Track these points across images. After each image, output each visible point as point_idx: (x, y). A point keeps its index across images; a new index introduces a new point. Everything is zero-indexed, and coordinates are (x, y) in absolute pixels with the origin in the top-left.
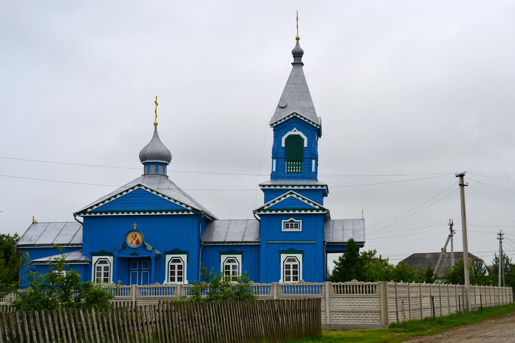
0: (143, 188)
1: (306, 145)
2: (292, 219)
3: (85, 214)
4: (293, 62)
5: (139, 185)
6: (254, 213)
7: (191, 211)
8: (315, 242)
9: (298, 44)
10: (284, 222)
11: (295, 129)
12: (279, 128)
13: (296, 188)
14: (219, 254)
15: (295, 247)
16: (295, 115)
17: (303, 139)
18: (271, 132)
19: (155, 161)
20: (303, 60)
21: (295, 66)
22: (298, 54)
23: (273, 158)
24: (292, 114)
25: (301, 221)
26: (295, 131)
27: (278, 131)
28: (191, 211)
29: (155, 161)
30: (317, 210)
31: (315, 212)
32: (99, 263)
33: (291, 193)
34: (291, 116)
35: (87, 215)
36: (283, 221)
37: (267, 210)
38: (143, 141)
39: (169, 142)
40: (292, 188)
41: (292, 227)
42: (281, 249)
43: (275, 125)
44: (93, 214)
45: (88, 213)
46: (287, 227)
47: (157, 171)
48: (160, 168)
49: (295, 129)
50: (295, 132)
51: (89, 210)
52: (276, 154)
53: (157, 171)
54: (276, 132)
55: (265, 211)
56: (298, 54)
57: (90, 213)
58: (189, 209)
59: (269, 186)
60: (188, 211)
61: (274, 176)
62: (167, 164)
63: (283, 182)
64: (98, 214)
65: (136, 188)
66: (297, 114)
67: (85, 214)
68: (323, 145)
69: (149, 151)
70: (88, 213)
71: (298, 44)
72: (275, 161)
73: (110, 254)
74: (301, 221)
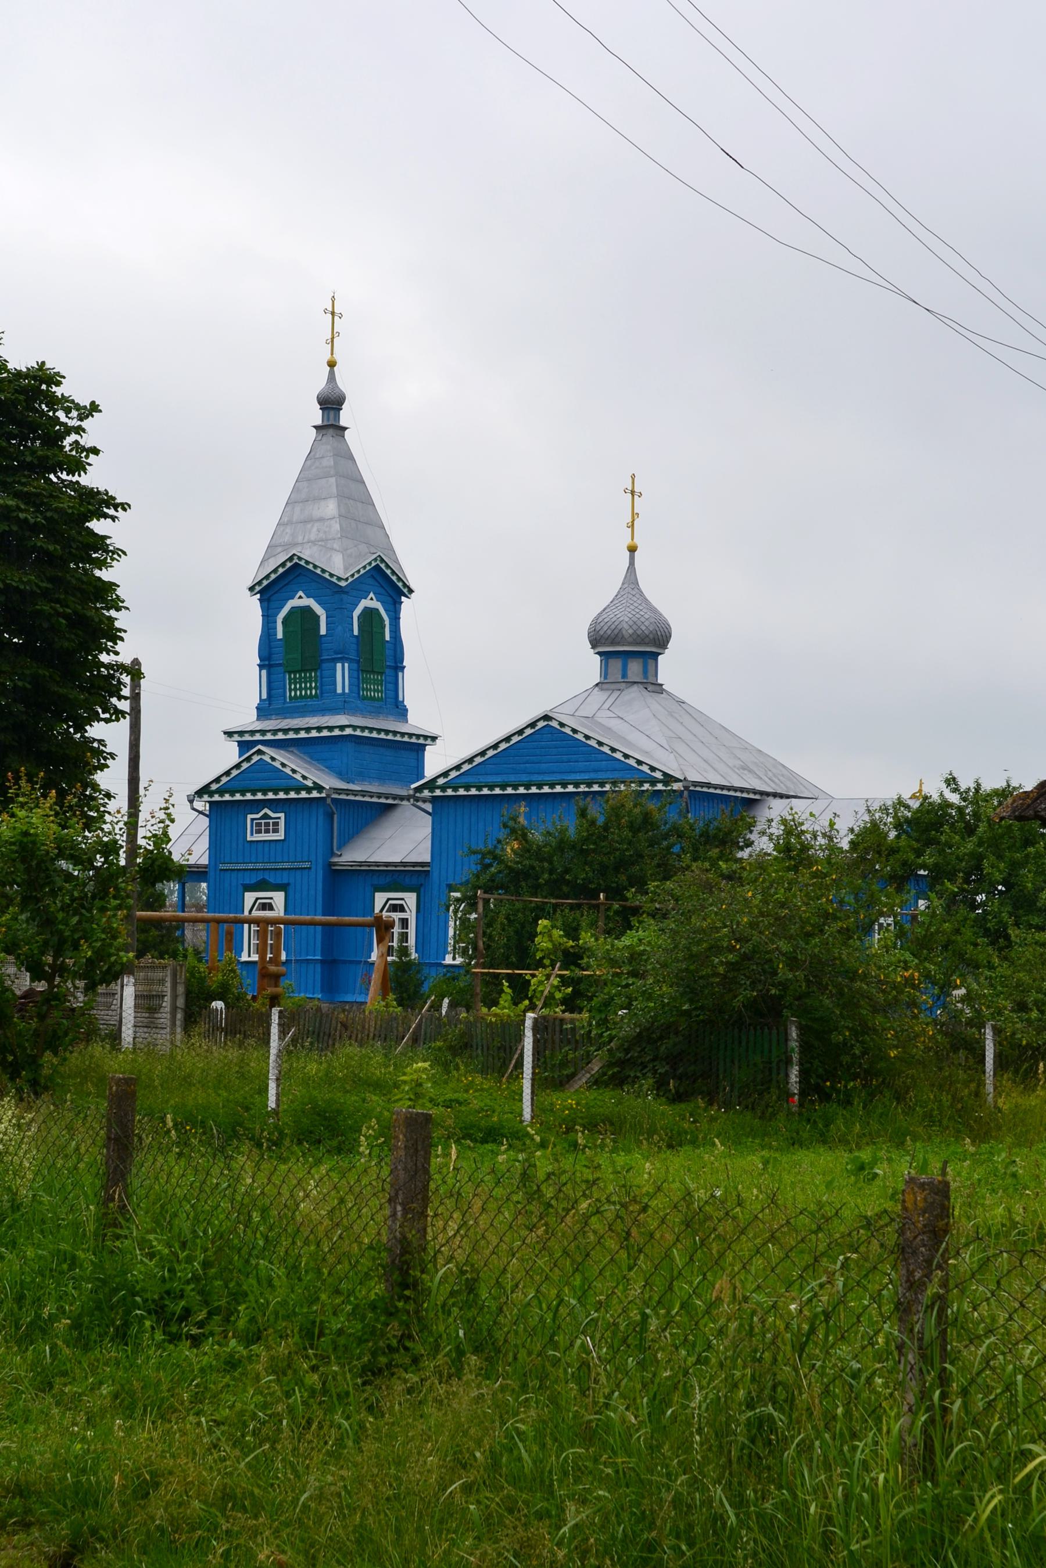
0: (554, 724)
1: (323, 631)
2: (266, 810)
3: (432, 790)
4: (319, 422)
5: (546, 717)
6: (191, 802)
7: (660, 781)
8: (307, 865)
9: (332, 378)
10: (252, 820)
11: (300, 593)
12: (270, 591)
13: (269, 737)
14: (241, 889)
15: (272, 878)
16: (296, 560)
17: (319, 617)
18: (254, 606)
19: (630, 650)
20: (317, 416)
21: (324, 432)
22: (331, 403)
23: (261, 667)
24: (291, 559)
25: (282, 815)
26: (300, 597)
27: (269, 600)
28: (660, 781)
29: (630, 650)
30: (309, 790)
31: (304, 794)
32: (258, 909)
33: (259, 752)
34: (289, 564)
35: (438, 793)
36: (250, 817)
37: (217, 791)
38: (595, 597)
39: (665, 595)
40: (261, 738)
41: (267, 831)
42: (247, 882)
43: (258, 588)
44: (450, 792)
45: (438, 787)
46: (259, 832)
47: (624, 675)
48: (635, 668)
49: (300, 593)
50: (301, 600)
51: (441, 781)
52: (269, 658)
53: (624, 675)
54: (266, 604)
55: (221, 792)
56: (331, 403)
57: (443, 788)
58: (658, 775)
59: (252, 733)
60: (654, 782)
61: (263, 711)
62: (655, 656)
63: (285, 724)
64: (462, 792)
65: (541, 724)
66: (300, 558)
67: (432, 790)
68: (414, 619)
69: (624, 618)
70: (438, 787)
71: (332, 378)
72: (264, 672)
73: (277, 888)
74: (282, 815)
